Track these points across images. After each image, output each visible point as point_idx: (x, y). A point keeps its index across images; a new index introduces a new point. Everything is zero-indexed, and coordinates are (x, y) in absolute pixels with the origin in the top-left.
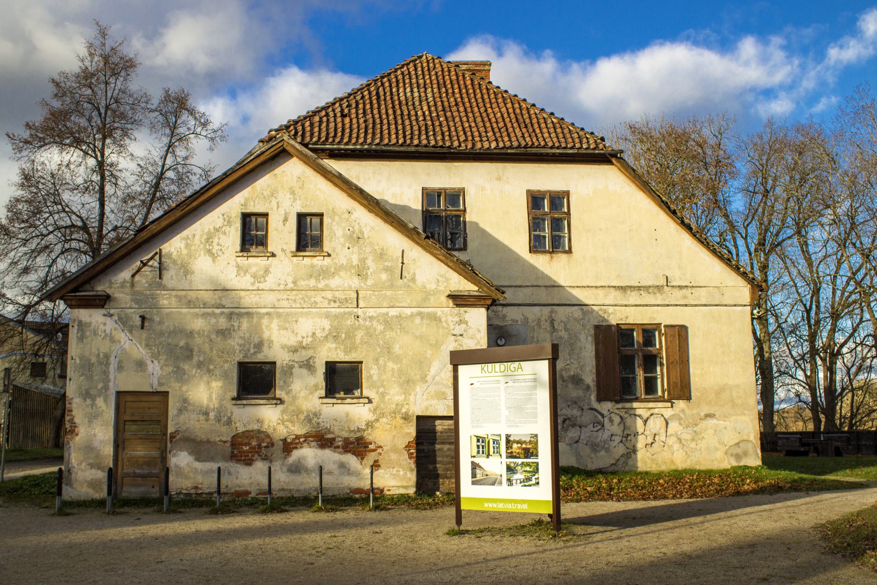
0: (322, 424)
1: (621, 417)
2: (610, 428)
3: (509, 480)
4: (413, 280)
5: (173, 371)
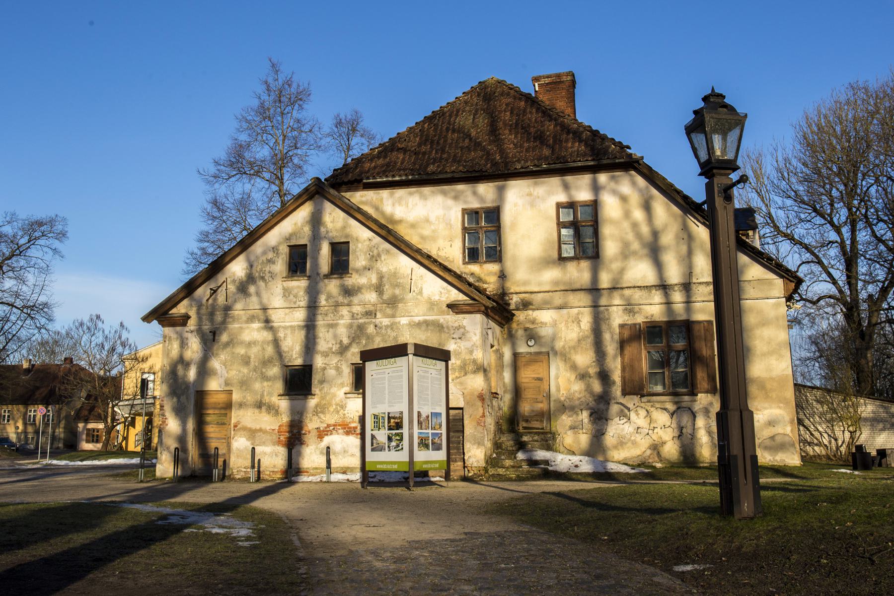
0: (347, 415)
1: (647, 410)
2: (636, 421)
3: (389, 447)
4: (420, 293)
5: (236, 374)
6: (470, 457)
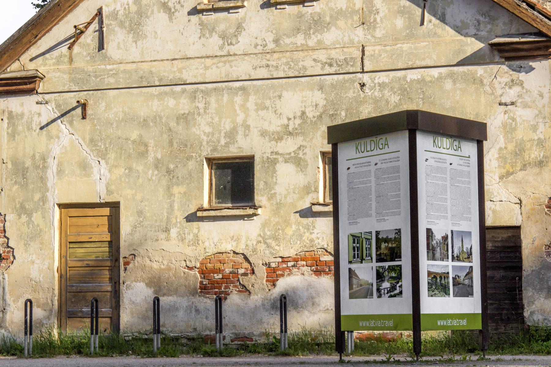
0: (316, 241)
3: (378, 290)
6: (532, 313)
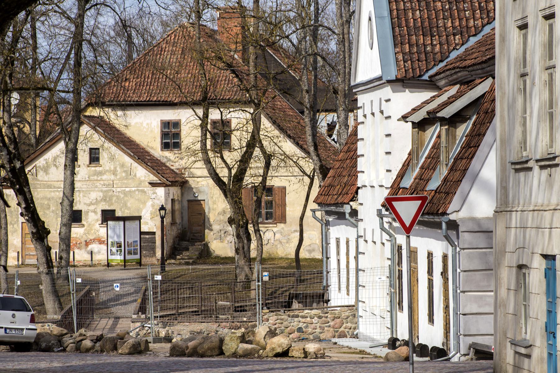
4: (135, 176)
